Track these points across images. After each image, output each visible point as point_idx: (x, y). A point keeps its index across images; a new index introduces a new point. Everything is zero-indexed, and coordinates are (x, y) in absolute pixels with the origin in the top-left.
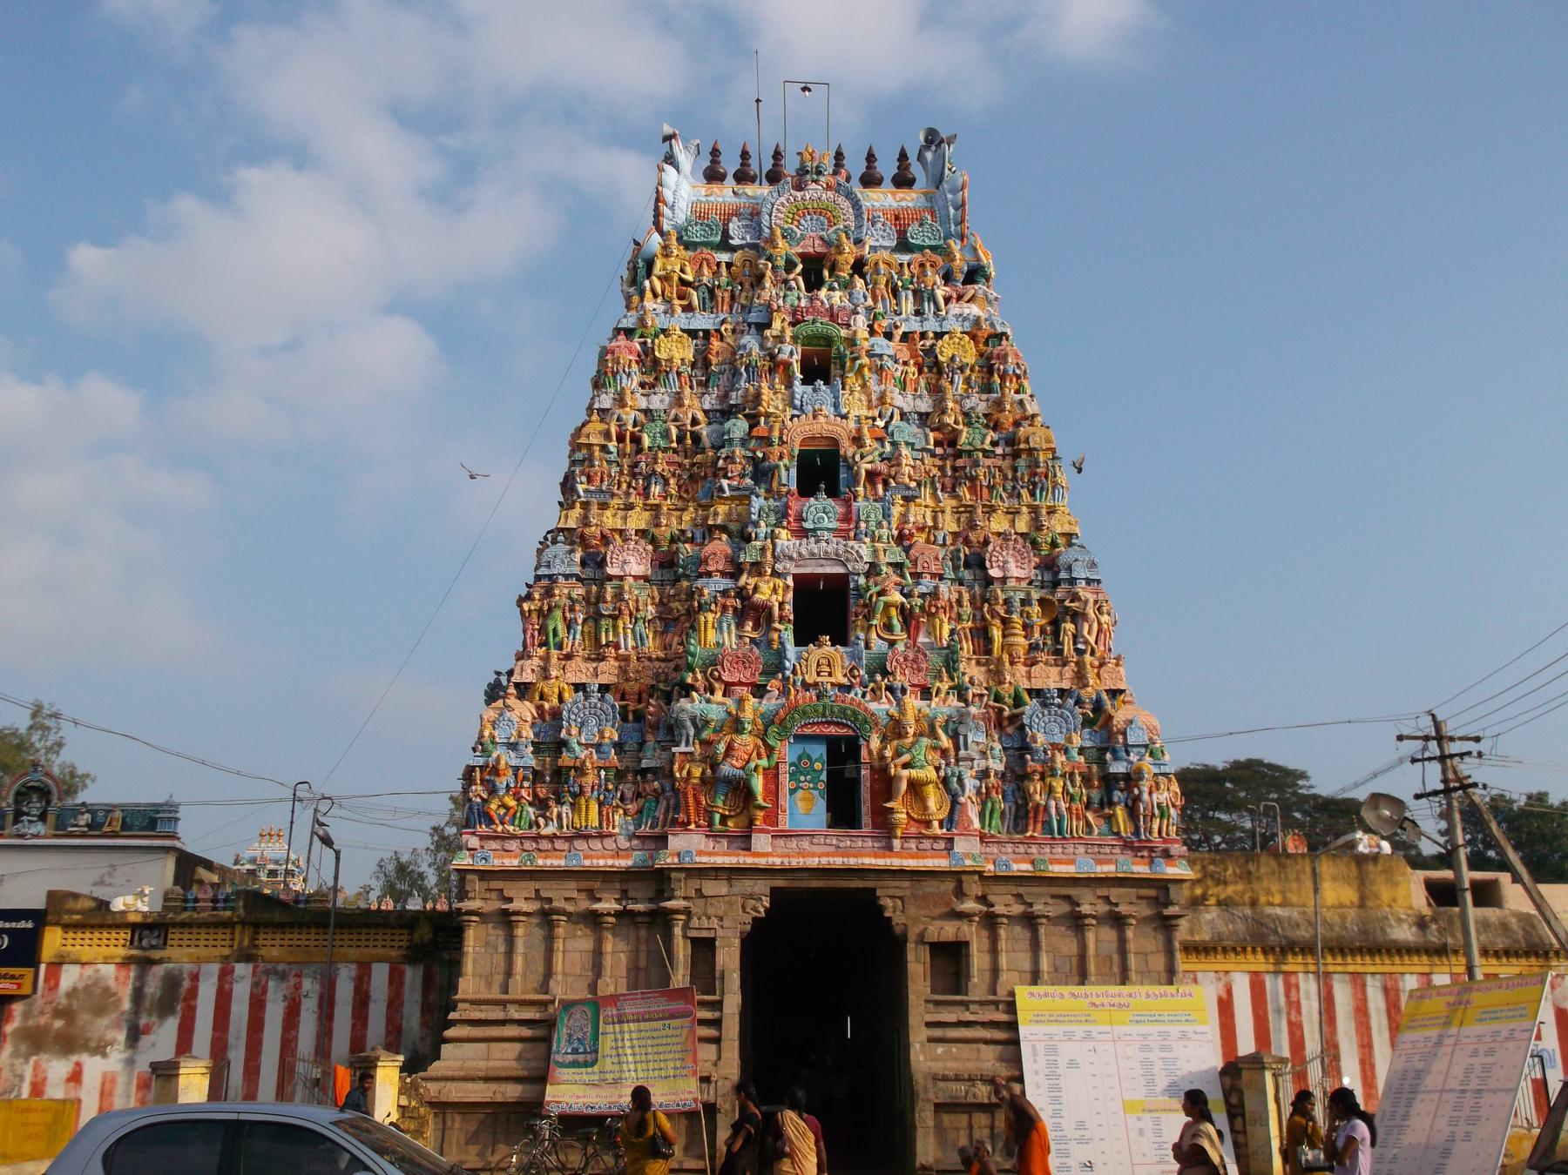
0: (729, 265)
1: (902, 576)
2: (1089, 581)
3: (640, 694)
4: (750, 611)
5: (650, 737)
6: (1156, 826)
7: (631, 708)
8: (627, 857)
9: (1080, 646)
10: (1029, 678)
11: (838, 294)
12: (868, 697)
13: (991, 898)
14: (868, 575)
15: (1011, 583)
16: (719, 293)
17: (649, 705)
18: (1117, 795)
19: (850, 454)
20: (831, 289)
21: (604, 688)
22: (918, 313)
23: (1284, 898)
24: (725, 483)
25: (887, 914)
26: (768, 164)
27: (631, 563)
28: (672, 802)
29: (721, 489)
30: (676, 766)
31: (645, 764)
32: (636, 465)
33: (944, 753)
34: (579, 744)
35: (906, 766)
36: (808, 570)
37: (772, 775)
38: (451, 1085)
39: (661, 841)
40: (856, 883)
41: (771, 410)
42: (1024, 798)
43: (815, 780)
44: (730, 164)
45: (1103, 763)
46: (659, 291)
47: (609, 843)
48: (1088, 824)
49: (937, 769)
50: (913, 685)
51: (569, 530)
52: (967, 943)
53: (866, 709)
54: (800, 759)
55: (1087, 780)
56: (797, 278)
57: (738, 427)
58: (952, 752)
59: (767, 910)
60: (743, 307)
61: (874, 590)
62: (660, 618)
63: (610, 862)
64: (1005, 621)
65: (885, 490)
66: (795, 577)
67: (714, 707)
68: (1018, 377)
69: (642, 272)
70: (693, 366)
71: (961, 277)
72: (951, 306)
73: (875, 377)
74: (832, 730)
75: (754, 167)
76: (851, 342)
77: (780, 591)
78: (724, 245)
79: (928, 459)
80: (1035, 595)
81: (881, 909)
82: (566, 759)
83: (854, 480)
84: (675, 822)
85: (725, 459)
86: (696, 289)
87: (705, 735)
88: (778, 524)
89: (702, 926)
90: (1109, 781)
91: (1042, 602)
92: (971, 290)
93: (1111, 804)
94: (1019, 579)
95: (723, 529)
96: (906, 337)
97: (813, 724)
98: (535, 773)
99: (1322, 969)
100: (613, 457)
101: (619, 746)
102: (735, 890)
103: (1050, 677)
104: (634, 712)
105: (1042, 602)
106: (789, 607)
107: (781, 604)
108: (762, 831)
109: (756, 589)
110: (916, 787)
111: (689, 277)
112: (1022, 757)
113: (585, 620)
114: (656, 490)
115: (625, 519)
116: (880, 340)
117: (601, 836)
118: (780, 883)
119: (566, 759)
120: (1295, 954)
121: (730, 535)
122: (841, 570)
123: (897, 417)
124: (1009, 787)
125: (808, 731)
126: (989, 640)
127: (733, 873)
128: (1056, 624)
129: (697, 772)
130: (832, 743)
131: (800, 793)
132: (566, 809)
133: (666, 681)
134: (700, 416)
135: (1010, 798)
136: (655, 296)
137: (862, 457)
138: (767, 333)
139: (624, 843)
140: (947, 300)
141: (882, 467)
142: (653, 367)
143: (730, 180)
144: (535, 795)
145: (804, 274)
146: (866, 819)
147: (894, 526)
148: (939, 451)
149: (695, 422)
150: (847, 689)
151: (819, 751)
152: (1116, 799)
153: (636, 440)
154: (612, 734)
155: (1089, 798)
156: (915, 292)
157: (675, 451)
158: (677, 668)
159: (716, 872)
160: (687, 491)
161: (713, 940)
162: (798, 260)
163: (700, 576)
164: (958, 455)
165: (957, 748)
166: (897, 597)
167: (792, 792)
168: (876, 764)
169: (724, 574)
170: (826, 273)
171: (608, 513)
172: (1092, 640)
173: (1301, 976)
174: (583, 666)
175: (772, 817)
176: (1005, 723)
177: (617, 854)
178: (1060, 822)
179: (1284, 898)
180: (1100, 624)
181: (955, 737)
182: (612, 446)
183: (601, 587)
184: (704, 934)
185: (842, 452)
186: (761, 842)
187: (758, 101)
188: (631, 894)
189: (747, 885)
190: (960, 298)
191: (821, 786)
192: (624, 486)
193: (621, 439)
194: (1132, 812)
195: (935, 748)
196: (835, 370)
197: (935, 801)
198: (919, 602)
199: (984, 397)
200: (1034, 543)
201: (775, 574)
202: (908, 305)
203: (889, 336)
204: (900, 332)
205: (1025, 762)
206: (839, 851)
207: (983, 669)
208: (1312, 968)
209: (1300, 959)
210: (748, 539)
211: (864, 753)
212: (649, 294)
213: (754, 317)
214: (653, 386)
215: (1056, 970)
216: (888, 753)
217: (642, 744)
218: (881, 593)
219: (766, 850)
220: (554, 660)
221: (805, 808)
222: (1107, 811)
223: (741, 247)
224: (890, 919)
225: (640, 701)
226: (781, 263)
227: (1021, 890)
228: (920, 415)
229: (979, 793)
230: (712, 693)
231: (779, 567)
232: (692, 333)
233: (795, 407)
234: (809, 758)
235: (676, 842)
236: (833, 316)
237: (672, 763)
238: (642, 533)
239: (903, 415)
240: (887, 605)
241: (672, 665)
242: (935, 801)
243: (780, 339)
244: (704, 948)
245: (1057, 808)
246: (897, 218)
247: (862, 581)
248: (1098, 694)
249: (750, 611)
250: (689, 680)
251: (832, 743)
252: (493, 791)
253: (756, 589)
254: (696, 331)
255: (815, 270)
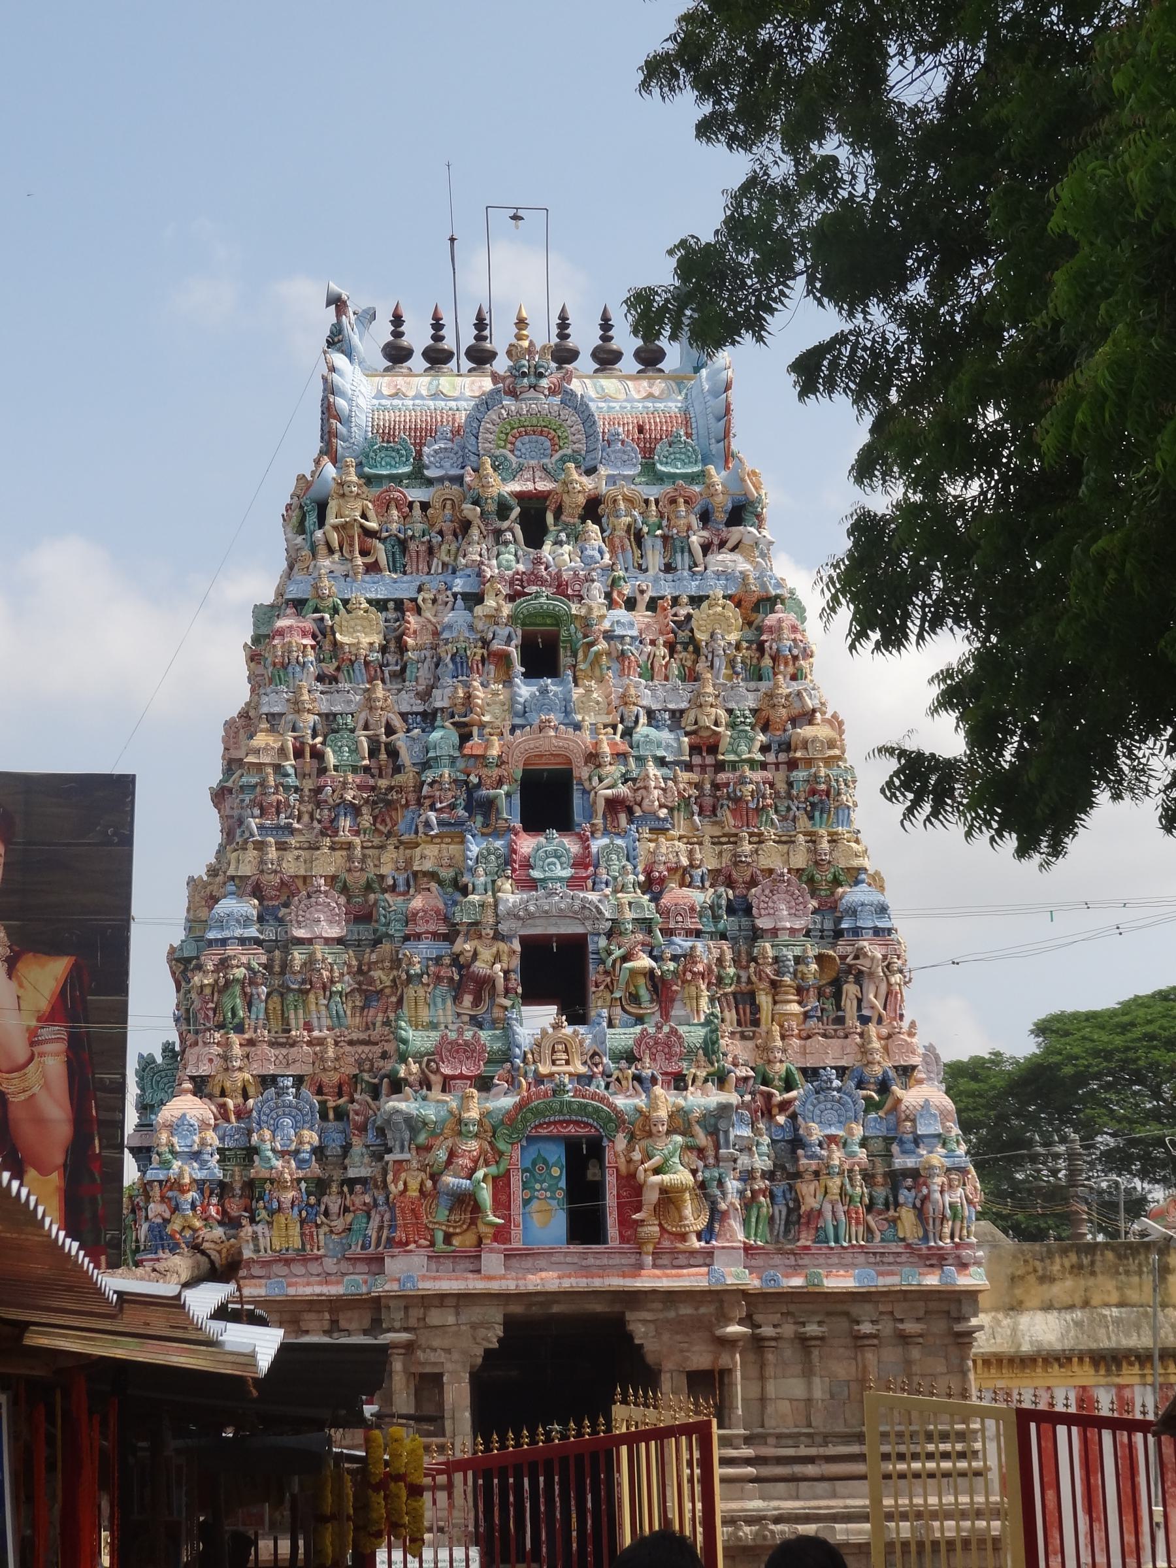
0: (425, 506)
1: (650, 931)
2: (877, 931)
3: (340, 1086)
4: (468, 984)
5: (356, 1141)
6: (947, 1230)
7: (331, 1104)
8: (338, 1283)
9: (865, 1012)
10: (804, 1054)
11: (567, 548)
12: (612, 1088)
13: (758, 1318)
14: (609, 935)
15: (784, 937)
16: (412, 546)
17: (351, 1102)
18: (904, 1196)
19: (585, 775)
20: (558, 543)
21: (299, 1080)
22: (669, 568)
23: (1122, 1295)
24: (432, 816)
25: (637, 1341)
26: (468, 338)
27: (323, 923)
28: (387, 1216)
29: (427, 824)
30: (390, 1177)
31: (352, 1173)
32: (319, 790)
33: (701, 1152)
34: (273, 1150)
35: (657, 1171)
36: (538, 931)
37: (501, 1184)
38: (1082, 1560)
39: (376, 1263)
40: (599, 1308)
41: (486, 718)
42: (796, 1200)
43: (552, 1189)
44: (417, 337)
45: (888, 1156)
46: (336, 545)
47: (314, 1268)
48: (869, 1230)
49: (694, 1172)
50: (665, 1074)
51: (243, 878)
52: (730, 1371)
53: (610, 1105)
54: (534, 1163)
55: (868, 1177)
56: (513, 530)
57: (442, 736)
58: (711, 1153)
59: (500, 1340)
60: (444, 565)
61: (618, 953)
62: (359, 990)
63: (318, 1290)
64: (774, 985)
65: (630, 822)
66: (524, 940)
67: (428, 1108)
68: (795, 658)
69: (312, 519)
70: (384, 649)
71: (721, 517)
72: (710, 557)
73: (616, 666)
74: (572, 1130)
75: (449, 344)
76: (586, 623)
77: (505, 958)
78: (418, 476)
79: (684, 776)
80: (812, 952)
81: (630, 1337)
82: (258, 1170)
83: (590, 814)
84: (391, 1242)
85: (431, 785)
86: (383, 540)
87: (422, 1138)
88: (499, 873)
89: (428, 1359)
90: (895, 1178)
91: (820, 959)
92: (736, 533)
93: (897, 1204)
94: (792, 931)
95: (433, 876)
96: (652, 605)
97: (549, 1124)
98: (222, 1184)
99: (1161, 1380)
100: (292, 781)
101: (319, 1151)
102: (463, 1318)
103: (830, 1054)
104: (336, 1109)
105: (820, 959)
106: (515, 977)
107: (506, 973)
108: (492, 1251)
109: (475, 954)
110: (669, 1198)
111: (373, 525)
112: (794, 1152)
113: (269, 995)
114: (345, 823)
115: (310, 862)
116: (621, 613)
117: (305, 1260)
118: (517, 1309)
119: (258, 1170)
120: (1131, 1364)
121: (440, 883)
122: (579, 930)
123: (643, 720)
124: (779, 1188)
125: (543, 1132)
126: (756, 1009)
127: (463, 1299)
128: (837, 984)
129: (414, 1185)
130: (572, 1146)
131: (535, 1205)
132: (259, 1228)
133: (371, 1070)
134: (397, 722)
135: (780, 1200)
136: (331, 551)
137: (601, 781)
138: (479, 610)
139: (330, 1264)
140: (706, 548)
141: (623, 790)
142: (336, 664)
143: (417, 362)
144: (224, 1213)
145: (523, 520)
146: (612, 1231)
147: (640, 869)
148: (697, 760)
149: (390, 730)
150: (589, 1079)
151: (556, 1154)
152: (901, 1200)
153: (318, 755)
154: (311, 1137)
155: (871, 1198)
156: (665, 538)
157: (367, 769)
158: (384, 1056)
159: (442, 1299)
160: (383, 821)
161: (441, 1375)
162: (513, 502)
163: (407, 938)
164: (720, 767)
165: (717, 1147)
166: (644, 962)
167: (526, 1202)
168: (623, 1169)
169: (435, 935)
170: (550, 518)
171: (290, 856)
172: (879, 1004)
173: (1137, 1389)
174: (272, 1052)
175: (501, 1234)
176: (775, 1111)
177: (326, 1278)
178: (836, 1228)
179: (1122, 1295)
180: (889, 984)
181: (713, 1133)
182: (289, 764)
183: (286, 951)
184: (428, 1370)
185: (576, 773)
186: (492, 1262)
187: (452, 240)
188: (343, 1324)
189: (475, 1313)
190: (722, 544)
191: (560, 1195)
192: (306, 818)
193: (299, 754)
194: (920, 1213)
195: (688, 1148)
196: (565, 659)
197: (693, 1218)
198: (671, 966)
199: (752, 685)
200: (811, 881)
201: (498, 937)
202: (655, 559)
203: (631, 604)
204: (646, 597)
205: (796, 1160)
206: (586, 1271)
207: (750, 1044)
208: (1149, 1379)
209: (1136, 1369)
210: (464, 891)
211: (608, 1156)
212: (322, 550)
213: (459, 585)
214: (334, 679)
215: (832, 1397)
216: (637, 1156)
217: (346, 1148)
218: (625, 958)
219: (497, 1276)
220: (237, 1050)
221: (547, 1220)
222: (891, 1213)
223: (441, 480)
224: (641, 1346)
225: (340, 1095)
226: (492, 507)
227: (792, 1308)
228: (673, 712)
229: (741, 1193)
230: (429, 1088)
231: (503, 928)
232: (380, 605)
233: (516, 715)
234: (545, 1162)
235: (395, 1265)
236: (561, 588)
237: (385, 1173)
238: (332, 880)
239: (650, 713)
240: (633, 972)
241: (378, 1050)
242: (693, 1218)
243: (493, 618)
244: (429, 1384)
245: (833, 1212)
246: (641, 430)
247: (603, 942)
248: (885, 1072)
249: (468, 984)
250: (402, 1074)
251: (572, 1146)
252: (176, 1209)
253: (475, 954)
254: (386, 601)
255: (535, 519)
